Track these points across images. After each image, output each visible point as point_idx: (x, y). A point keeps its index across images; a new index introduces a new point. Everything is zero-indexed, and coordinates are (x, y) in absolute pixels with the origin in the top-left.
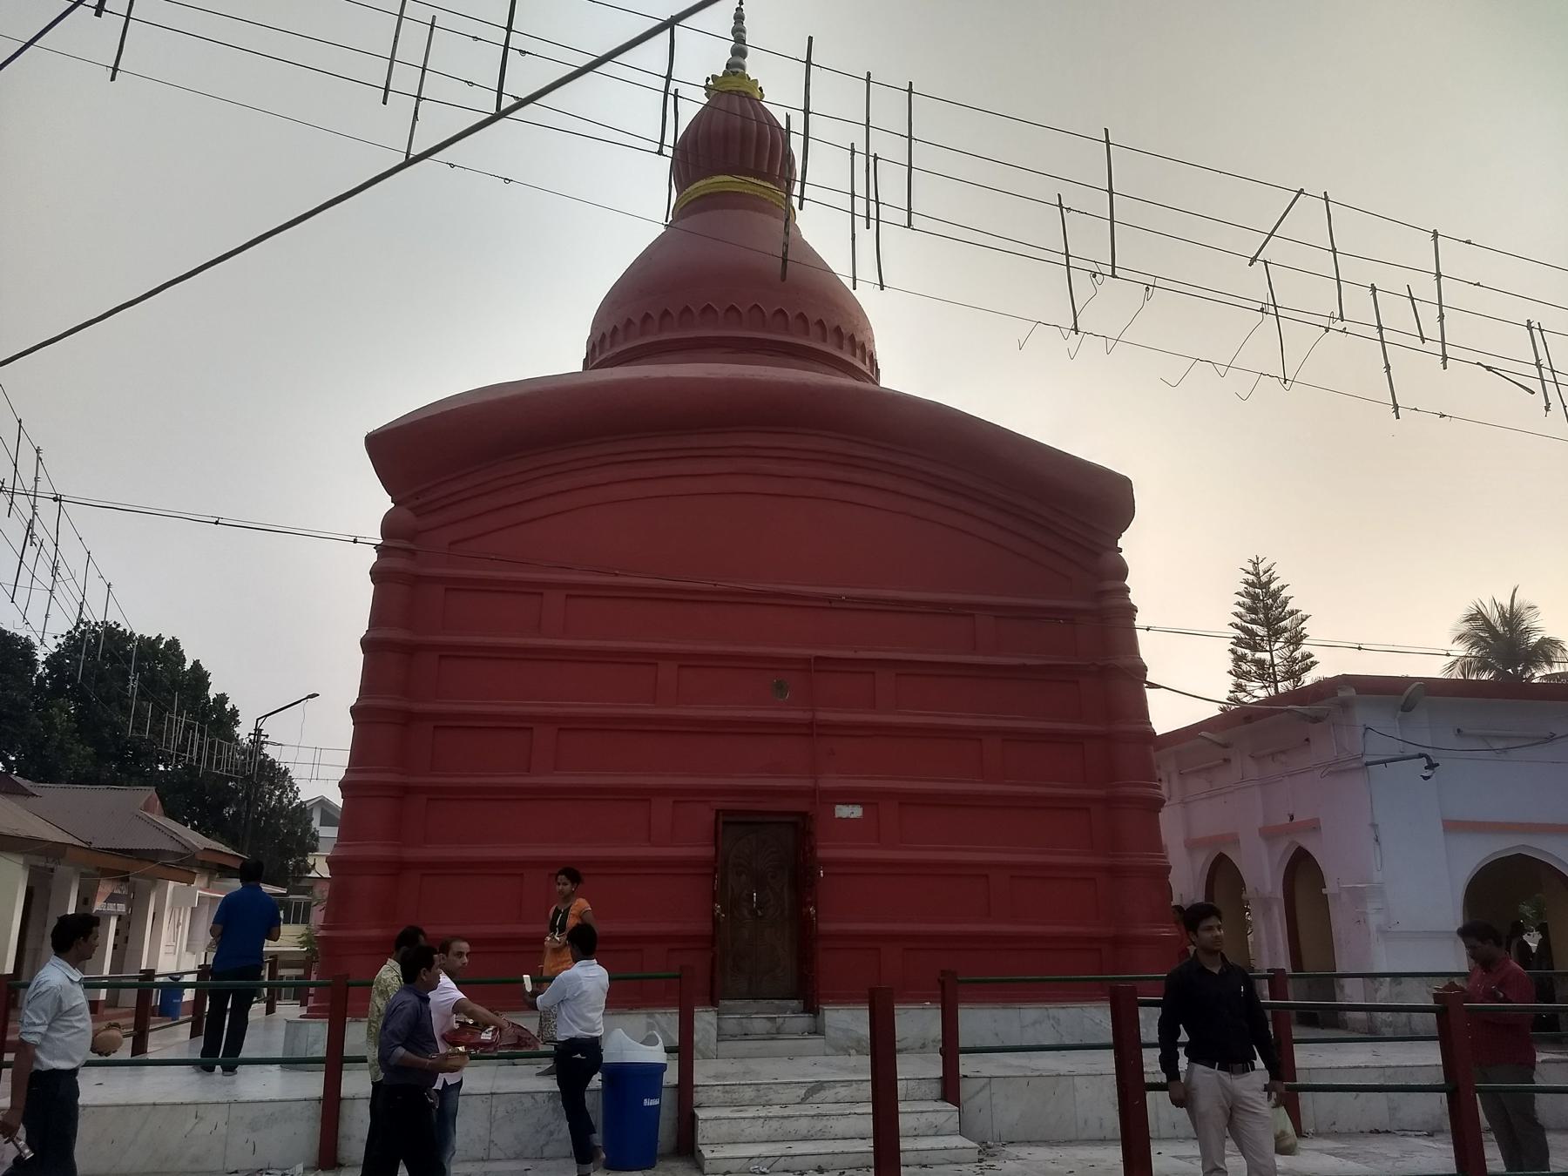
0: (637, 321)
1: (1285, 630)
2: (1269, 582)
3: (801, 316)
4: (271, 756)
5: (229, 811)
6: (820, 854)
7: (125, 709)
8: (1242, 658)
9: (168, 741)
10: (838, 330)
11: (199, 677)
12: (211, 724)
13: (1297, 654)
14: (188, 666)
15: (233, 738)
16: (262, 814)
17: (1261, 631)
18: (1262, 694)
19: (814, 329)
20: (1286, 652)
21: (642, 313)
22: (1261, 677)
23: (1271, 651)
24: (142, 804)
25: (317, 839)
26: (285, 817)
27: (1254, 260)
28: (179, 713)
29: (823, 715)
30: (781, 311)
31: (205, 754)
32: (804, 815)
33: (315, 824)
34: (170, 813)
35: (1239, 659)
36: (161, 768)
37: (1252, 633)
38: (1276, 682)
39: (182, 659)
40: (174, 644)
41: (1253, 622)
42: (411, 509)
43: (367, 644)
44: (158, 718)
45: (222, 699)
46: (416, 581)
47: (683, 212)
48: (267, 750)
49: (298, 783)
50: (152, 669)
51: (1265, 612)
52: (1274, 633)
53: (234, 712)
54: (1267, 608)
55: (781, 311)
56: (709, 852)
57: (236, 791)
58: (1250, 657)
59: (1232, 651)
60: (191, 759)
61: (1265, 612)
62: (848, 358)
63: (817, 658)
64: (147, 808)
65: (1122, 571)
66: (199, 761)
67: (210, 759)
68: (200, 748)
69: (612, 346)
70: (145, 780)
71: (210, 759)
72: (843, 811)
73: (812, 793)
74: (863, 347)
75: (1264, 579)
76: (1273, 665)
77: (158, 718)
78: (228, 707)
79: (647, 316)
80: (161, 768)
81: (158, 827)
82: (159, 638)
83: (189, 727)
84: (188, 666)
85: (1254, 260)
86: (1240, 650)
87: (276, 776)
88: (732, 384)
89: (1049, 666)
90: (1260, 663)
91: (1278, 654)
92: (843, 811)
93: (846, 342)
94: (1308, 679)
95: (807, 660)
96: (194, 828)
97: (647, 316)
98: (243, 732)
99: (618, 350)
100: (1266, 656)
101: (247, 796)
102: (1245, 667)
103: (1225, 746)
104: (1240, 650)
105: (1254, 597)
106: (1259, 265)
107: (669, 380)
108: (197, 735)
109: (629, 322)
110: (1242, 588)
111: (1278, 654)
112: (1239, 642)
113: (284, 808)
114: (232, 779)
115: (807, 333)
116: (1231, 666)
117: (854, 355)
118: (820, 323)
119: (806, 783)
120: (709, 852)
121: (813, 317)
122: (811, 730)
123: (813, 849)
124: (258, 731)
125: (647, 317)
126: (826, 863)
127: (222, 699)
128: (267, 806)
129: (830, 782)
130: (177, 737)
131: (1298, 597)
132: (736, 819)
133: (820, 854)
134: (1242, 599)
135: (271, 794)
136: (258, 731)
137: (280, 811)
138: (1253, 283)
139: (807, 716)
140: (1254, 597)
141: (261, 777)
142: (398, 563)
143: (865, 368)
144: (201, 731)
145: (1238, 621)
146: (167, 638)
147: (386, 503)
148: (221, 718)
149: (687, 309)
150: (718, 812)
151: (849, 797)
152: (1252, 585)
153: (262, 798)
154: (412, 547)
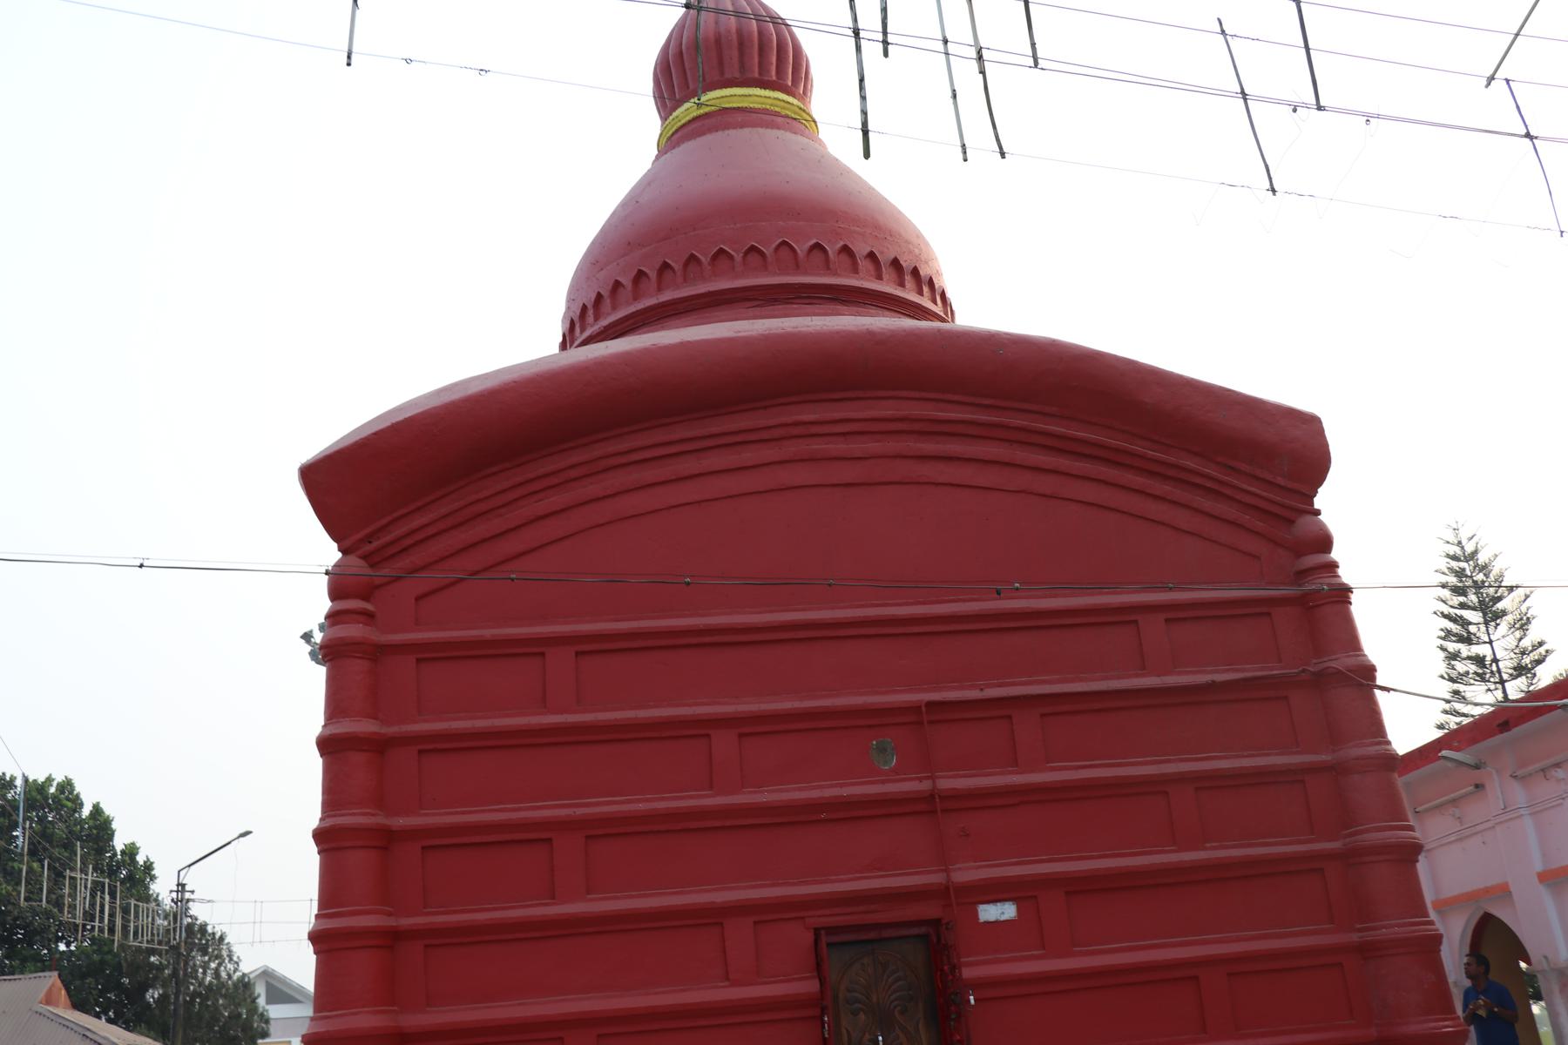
0: (626, 281)
1: (1504, 613)
2: (1475, 552)
3: (846, 250)
4: (201, 919)
5: (152, 995)
6: (967, 973)
7: (13, 877)
8: (1453, 656)
9: (72, 907)
10: (896, 263)
11: (101, 826)
12: (123, 882)
13: (1526, 643)
14: (86, 812)
15: (146, 897)
16: (195, 994)
17: (1474, 616)
18: (1489, 698)
19: (864, 265)
20: (1511, 641)
21: (636, 271)
22: (1482, 678)
23: (1491, 642)
24: (42, 995)
25: (267, 1021)
26: (225, 996)
27: (1491, 78)
28: (84, 871)
29: (945, 784)
30: (818, 246)
31: (119, 922)
32: (936, 923)
33: (261, 1001)
34: (79, 1005)
35: (1453, 656)
36: (62, 947)
37: (1465, 623)
38: (1502, 682)
39: (77, 803)
40: (67, 786)
41: (1463, 606)
42: (364, 557)
43: (326, 745)
44: (57, 875)
45: (131, 851)
46: (376, 653)
47: (670, 142)
48: (196, 910)
49: (238, 951)
50: (42, 820)
51: (1475, 593)
52: (1492, 616)
53: (148, 867)
54: (1478, 586)
55: (818, 246)
56: (810, 986)
57: (160, 968)
58: (1465, 653)
59: (1443, 649)
60: (101, 930)
61: (1475, 593)
62: (912, 297)
63: (929, 704)
64: (49, 1000)
65: (1324, 542)
66: (112, 930)
67: (125, 928)
68: (112, 915)
69: (597, 318)
70: (43, 965)
71: (125, 928)
72: (991, 912)
73: (943, 893)
74: (931, 283)
75: (1469, 548)
76: (1495, 660)
77: (57, 875)
78: (140, 859)
79: (641, 274)
80: (62, 947)
81: (66, 1025)
82: (49, 780)
83: (97, 887)
84: (86, 812)
85: (1491, 78)
86: (1452, 646)
87: (202, 941)
88: (768, 339)
89: (1245, 680)
90: (1479, 660)
91: (1502, 644)
92: (991, 912)
93: (908, 278)
94: (1546, 676)
95: (915, 709)
96: (110, 1021)
97: (641, 274)
98: (163, 888)
99: (604, 322)
100: (1483, 650)
101: (175, 974)
102: (1461, 667)
103: (1477, 767)
104: (1452, 646)
105: (1460, 574)
106: (1498, 84)
107: (684, 345)
108: (107, 897)
109: (617, 284)
110: (1444, 564)
111: (1502, 644)
112: (1448, 635)
113: (223, 985)
114: (153, 952)
115: (855, 269)
116: (1442, 668)
117: (921, 293)
118: (872, 256)
119: (936, 878)
120: (810, 986)
121: (861, 249)
122: (931, 805)
123: (954, 967)
124: (181, 887)
125: (640, 275)
126: (977, 985)
127: (131, 851)
128: (201, 984)
129: (966, 874)
130: (83, 895)
131: (1511, 563)
132: (841, 935)
133: (967, 973)
134: (1444, 579)
135: (205, 967)
136: (181, 887)
137: (217, 989)
138: (1495, 108)
139: (925, 786)
140: (1460, 574)
141: (191, 946)
142: (354, 631)
143: (938, 309)
144: (113, 895)
145: (1447, 610)
146: (59, 778)
147: (330, 553)
148: (132, 875)
149: (692, 258)
150: (817, 931)
151: (996, 891)
152: (1455, 558)
153: (194, 975)
154: (369, 606)
